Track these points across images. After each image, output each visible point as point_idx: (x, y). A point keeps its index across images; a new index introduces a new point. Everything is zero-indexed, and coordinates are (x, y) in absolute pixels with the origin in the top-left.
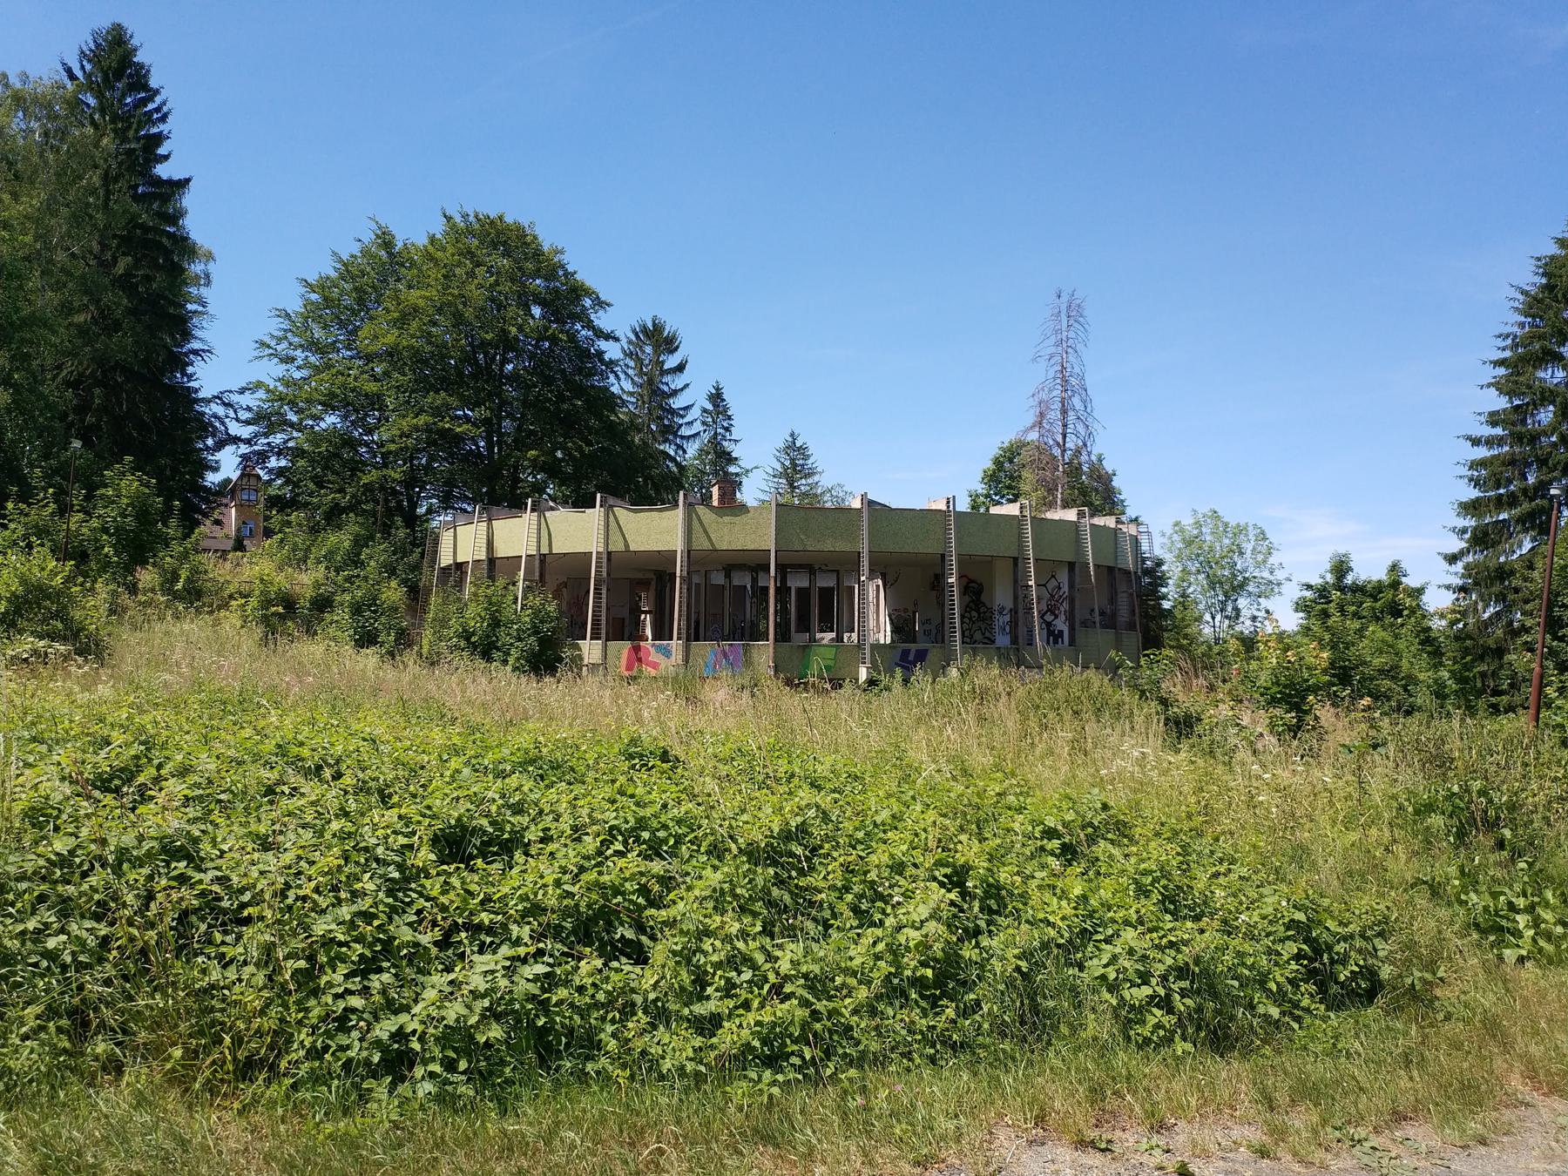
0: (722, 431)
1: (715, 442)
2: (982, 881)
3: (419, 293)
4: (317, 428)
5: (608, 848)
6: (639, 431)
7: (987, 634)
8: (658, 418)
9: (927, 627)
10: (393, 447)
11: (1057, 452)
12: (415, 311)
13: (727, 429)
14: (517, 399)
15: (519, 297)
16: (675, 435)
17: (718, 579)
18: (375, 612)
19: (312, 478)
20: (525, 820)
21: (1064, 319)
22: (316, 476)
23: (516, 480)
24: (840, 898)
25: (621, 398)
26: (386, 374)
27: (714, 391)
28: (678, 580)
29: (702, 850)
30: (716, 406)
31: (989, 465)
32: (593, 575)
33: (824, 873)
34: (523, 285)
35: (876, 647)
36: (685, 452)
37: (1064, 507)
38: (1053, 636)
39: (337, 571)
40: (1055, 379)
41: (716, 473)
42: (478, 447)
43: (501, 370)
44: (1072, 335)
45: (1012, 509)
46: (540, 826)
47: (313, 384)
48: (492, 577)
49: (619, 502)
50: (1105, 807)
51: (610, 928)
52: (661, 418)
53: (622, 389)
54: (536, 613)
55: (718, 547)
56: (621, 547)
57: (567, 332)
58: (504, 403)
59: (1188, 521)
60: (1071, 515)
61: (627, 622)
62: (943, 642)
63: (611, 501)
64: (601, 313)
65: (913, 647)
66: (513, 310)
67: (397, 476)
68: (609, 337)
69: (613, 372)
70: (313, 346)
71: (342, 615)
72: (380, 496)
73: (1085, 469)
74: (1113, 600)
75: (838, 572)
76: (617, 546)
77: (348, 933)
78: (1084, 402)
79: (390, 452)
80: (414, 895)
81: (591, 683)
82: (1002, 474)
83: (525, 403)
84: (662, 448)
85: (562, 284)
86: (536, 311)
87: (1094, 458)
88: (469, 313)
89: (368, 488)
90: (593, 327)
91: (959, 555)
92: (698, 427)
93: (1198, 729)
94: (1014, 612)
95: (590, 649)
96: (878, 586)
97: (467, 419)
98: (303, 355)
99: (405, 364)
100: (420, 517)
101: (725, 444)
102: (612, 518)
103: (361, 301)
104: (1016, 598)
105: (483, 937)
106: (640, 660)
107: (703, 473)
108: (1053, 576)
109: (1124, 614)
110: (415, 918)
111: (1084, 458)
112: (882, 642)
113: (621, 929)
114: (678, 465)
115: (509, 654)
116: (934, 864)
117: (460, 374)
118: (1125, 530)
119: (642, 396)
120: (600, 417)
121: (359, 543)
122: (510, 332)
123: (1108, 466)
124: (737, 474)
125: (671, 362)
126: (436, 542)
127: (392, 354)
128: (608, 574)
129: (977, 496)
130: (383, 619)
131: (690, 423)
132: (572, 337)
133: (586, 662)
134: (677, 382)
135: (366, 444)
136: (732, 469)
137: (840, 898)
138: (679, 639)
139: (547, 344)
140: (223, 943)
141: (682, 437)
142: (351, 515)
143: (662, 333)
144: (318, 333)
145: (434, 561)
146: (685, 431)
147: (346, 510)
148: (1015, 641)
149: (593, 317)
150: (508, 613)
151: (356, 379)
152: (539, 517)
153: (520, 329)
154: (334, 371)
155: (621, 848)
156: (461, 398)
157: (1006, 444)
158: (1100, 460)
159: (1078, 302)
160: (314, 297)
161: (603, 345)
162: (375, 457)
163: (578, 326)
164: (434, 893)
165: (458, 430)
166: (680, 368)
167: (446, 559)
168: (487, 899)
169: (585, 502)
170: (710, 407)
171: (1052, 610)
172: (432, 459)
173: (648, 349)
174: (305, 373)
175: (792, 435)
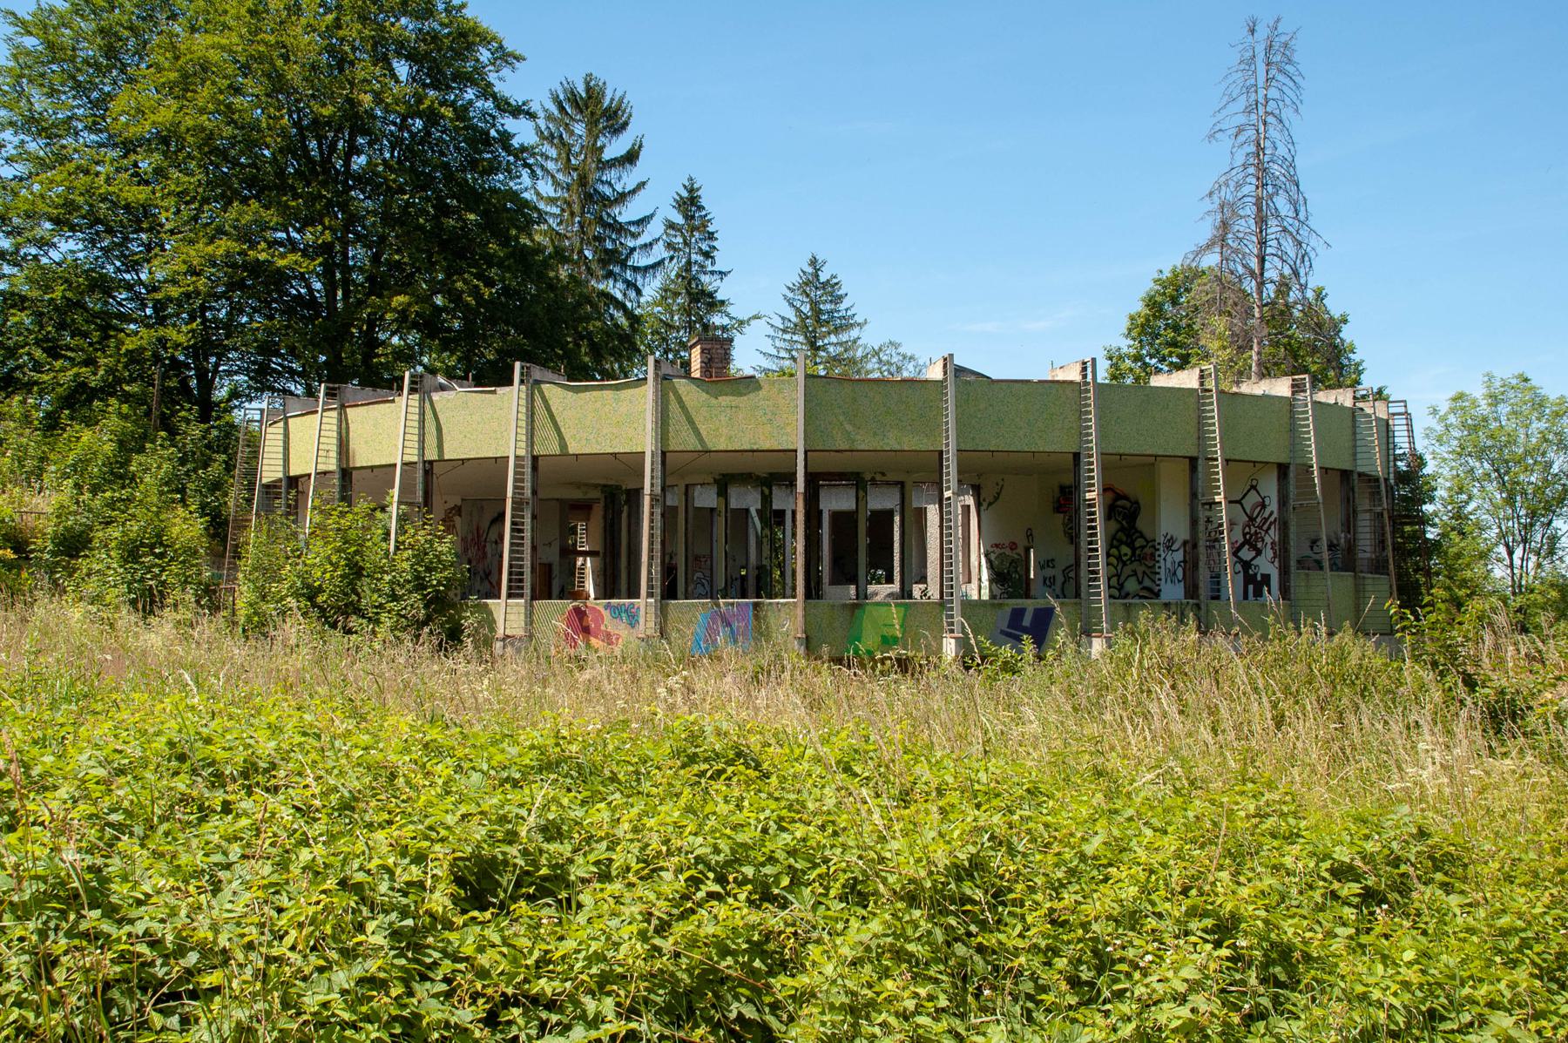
0: (700, 258)
1: (688, 276)
2: (1262, 939)
3: (209, 39)
4: (44, 260)
5: (698, 889)
6: (566, 260)
7: (1147, 583)
8: (596, 238)
9: (1049, 572)
10: (175, 292)
11: (1250, 285)
12: (205, 70)
13: (707, 255)
14: (375, 213)
15: (375, 46)
16: (624, 264)
17: (706, 498)
18: (161, 556)
19: (38, 343)
20: (566, 849)
21: (1261, 68)
22: (47, 340)
23: (372, 343)
24: (1049, 964)
25: (536, 209)
26: (159, 172)
27: (685, 194)
28: (647, 501)
29: (833, 893)
30: (689, 217)
31: (1138, 307)
32: (510, 493)
33: (1019, 927)
34: (382, 28)
35: (969, 607)
36: (639, 292)
37: (1262, 376)
38: (1254, 584)
39: (95, 490)
40: (1245, 167)
41: (690, 327)
42: (310, 290)
43: (347, 164)
44: (1273, 93)
45: (1187, 379)
46: (592, 858)
47: (36, 187)
48: (346, 497)
49: (549, 375)
50: (1422, 834)
51: (719, 1003)
52: (599, 239)
53: (538, 194)
54: (420, 555)
55: (711, 446)
56: (554, 448)
57: (453, 104)
58: (352, 219)
59: (1478, 392)
60: (1281, 387)
61: (556, 570)
62: (1078, 595)
63: (537, 372)
64: (506, 72)
65: (1030, 605)
66: (364, 68)
67: (182, 339)
68: (516, 111)
69: (526, 165)
70: (33, 124)
71: (103, 561)
72: (156, 371)
73: (1296, 313)
74: (1349, 524)
75: (902, 484)
76: (547, 446)
77: (351, 1008)
78: (1295, 205)
79: (170, 299)
80: (437, 955)
81: (514, 669)
82: (1161, 323)
83: (387, 219)
84: (601, 287)
85: (441, 24)
86: (402, 69)
87: (1310, 295)
88: (293, 73)
89: (134, 357)
90: (494, 96)
91: (1103, 454)
92: (659, 252)
93: (1532, 720)
94: (1191, 545)
95: (507, 613)
96: (966, 509)
97: (292, 246)
98: (16, 140)
99: (189, 156)
100: (217, 404)
101: (705, 279)
102: (427, 405)
103: (110, 52)
104: (1194, 522)
105: (544, 1015)
106: (586, 631)
107: (669, 326)
108: (1253, 487)
109: (1366, 547)
110: (444, 987)
111: (1294, 295)
112: (975, 597)
113: (736, 1005)
114: (629, 314)
115: (378, 622)
116: (1187, 914)
117: (281, 173)
118: (1369, 411)
119: (569, 204)
120: (505, 241)
121: (129, 446)
122: (360, 104)
123: (1334, 306)
124: (724, 328)
125: (615, 148)
126: (254, 445)
127: (165, 139)
128: (534, 492)
129: (1121, 358)
130: (174, 568)
131: (648, 246)
132: (462, 113)
133: (500, 633)
134: (626, 179)
135: (129, 287)
136: (717, 320)
137: (1049, 964)
138: (650, 595)
139: (419, 123)
140: (164, 1029)
141: (636, 269)
142: (112, 401)
143: (599, 102)
144: (40, 102)
145: (252, 473)
146: (640, 260)
147: (94, 393)
148: (1192, 591)
149: (492, 77)
150: (373, 557)
151: (108, 181)
152: (422, 401)
153: (378, 98)
154: (71, 167)
155: (717, 888)
156: (284, 209)
157: (1167, 274)
158: (1320, 296)
159: (1283, 39)
160: (30, 42)
161: (510, 124)
162: (144, 306)
163: (470, 94)
164: (468, 950)
165: (281, 263)
166: (631, 157)
167: (270, 470)
168: (544, 961)
169: (493, 376)
170: (679, 219)
171: (1251, 542)
172: (236, 309)
173: (579, 129)
174: (20, 169)
175: (813, 262)
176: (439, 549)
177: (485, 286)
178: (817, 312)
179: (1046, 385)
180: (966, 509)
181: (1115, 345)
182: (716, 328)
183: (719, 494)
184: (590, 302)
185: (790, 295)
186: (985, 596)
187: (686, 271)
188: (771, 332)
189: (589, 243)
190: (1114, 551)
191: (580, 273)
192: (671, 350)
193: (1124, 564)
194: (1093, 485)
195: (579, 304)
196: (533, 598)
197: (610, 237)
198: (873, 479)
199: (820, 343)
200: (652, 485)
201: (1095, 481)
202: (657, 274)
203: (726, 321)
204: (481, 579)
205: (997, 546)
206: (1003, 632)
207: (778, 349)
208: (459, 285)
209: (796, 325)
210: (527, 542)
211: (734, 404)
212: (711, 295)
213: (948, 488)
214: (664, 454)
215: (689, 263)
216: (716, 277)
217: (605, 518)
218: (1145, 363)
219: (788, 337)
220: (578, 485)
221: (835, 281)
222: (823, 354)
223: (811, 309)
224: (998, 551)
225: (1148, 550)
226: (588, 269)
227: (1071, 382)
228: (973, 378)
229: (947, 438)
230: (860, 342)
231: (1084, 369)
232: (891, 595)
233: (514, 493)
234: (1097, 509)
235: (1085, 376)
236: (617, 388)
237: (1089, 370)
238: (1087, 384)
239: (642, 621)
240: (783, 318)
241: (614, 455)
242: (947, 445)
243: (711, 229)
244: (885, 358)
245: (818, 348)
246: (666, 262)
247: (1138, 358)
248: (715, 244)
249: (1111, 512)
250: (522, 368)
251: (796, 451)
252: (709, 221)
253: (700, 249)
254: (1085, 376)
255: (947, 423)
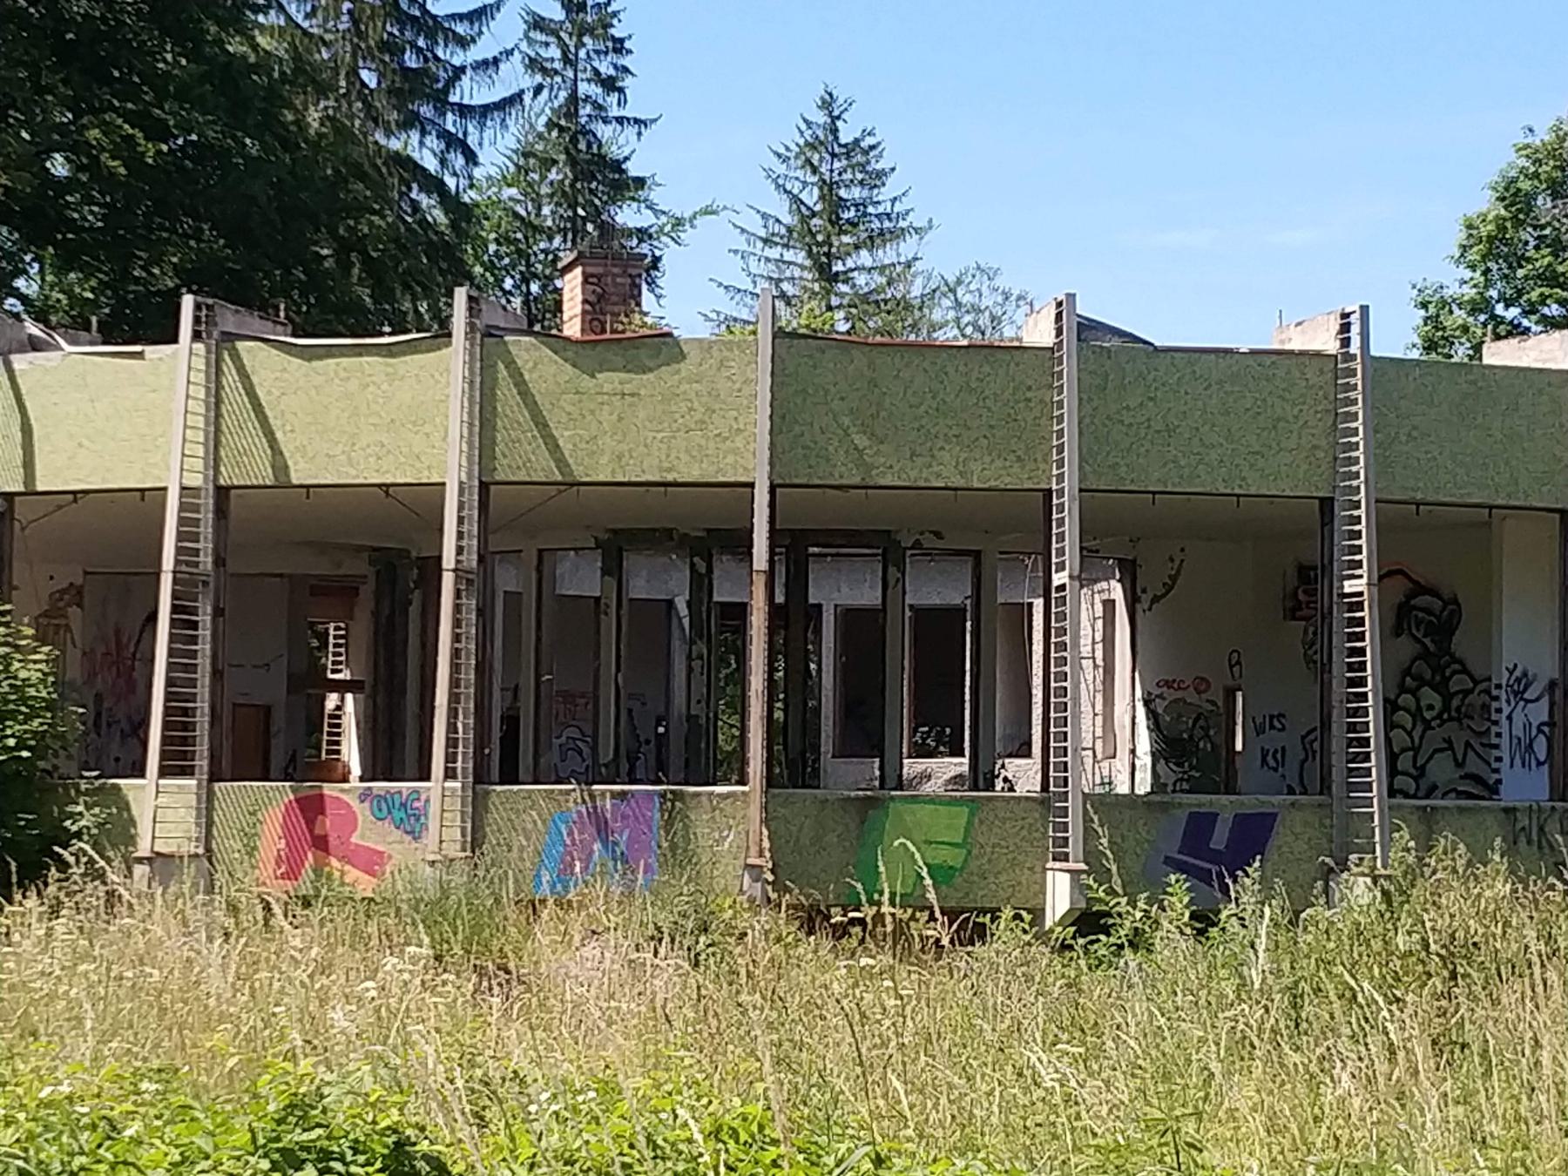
0: (595, 90)
8: (385, 46)
9: (1272, 740)
13: (610, 85)
16: (441, 101)
28: (448, 580)
31: (1484, 203)
35: (1105, 804)
36: (471, 158)
41: (574, 230)
49: (255, 324)
52: (393, 48)
55: (581, 474)
56: (262, 473)
61: (279, 720)
63: (229, 318)
65: (1225, 806)
75: (977, 555)
82: (1528, 234)
84: (395, 144)
92: (513, 77)
96: (1109, 605)
101: (604, 131)
106: (321, 844)
107: (535, 229)
112: (1123, 788)
114: (449, 201)
124: (643, 234)
128: (219, 561)
129: (1443, 303)
136: (628, 216)
141: (464, 110)
146: (472, 91)
157: (1543, 136)
175: (827, 103)
176: (23, 674)
177: (147, 139)
178: (833, 204)
179: (1268, 360)
180: (1109, 605)
181: (1434, 279)
182: (629, 233)
183: (605, 572)
184: (363, 177)
185: (781, 169)
186: (1144, 786)
187: (568, 116)
188: (741, 243)
189: (369, 55)
190: (1406, 699)
191: (352, 117)
192: (535, 276)
193: (1427, 726)
194: (1359, 564)
195: (340, 180)
196: (214, 777)
197: (413, 45)
198: (917, 545)
199: (838, 267)
200: (460, 551)
201: (1363, 557)
202: (510, 122)
203: (644, 219)
204: (123, 735)
205: (1168, 684)
206: (1168, 861)
207: (754, 278)
208: (94, 133)
209: (790, 230)
210: (204, 663)
211: (628, 388)
212: (617, 166)
213: (1061, 567)
214: (484, 487)
215: (573, 99)
216: (631, 131)
217: (376, 614)
218: (1493, 317)
219: (774, 253)
220: (321, 547)
221: (869, 141)
222: (844, 288)
223: (822, 198)
224: (1171, 695)
225: (1475, 699)
226: (368, 106)
227: (1318, 354)
228: (1116, 342)
229: (1060, 464)
230: (918, 266)
231: (1345, 328)
232: (957, 779)
233: (177, 562)
234: (1365, 613)
235: (1346, 343)
236: (389, 351)
237: (886, 339)
238: (1350, 357)
239: (433, 825)
240: (765, 216)
241: (385, 487)
242: (1060, 478)
243: (616, 32)
244: (967, 299)
245: (835, 278)
246: (527, 98)
247: (1479, 306)
248: (626, 61)
249: (1399, 620)
250: (198, 307)
251: (752, 485)
252: (615, 14)
253: (596, 72)
254: (1346, 343)
255: (1060, 434)
